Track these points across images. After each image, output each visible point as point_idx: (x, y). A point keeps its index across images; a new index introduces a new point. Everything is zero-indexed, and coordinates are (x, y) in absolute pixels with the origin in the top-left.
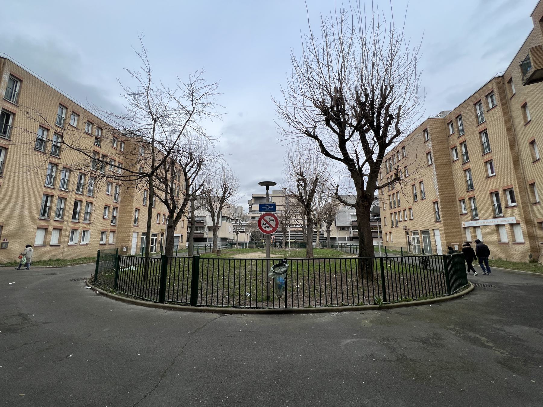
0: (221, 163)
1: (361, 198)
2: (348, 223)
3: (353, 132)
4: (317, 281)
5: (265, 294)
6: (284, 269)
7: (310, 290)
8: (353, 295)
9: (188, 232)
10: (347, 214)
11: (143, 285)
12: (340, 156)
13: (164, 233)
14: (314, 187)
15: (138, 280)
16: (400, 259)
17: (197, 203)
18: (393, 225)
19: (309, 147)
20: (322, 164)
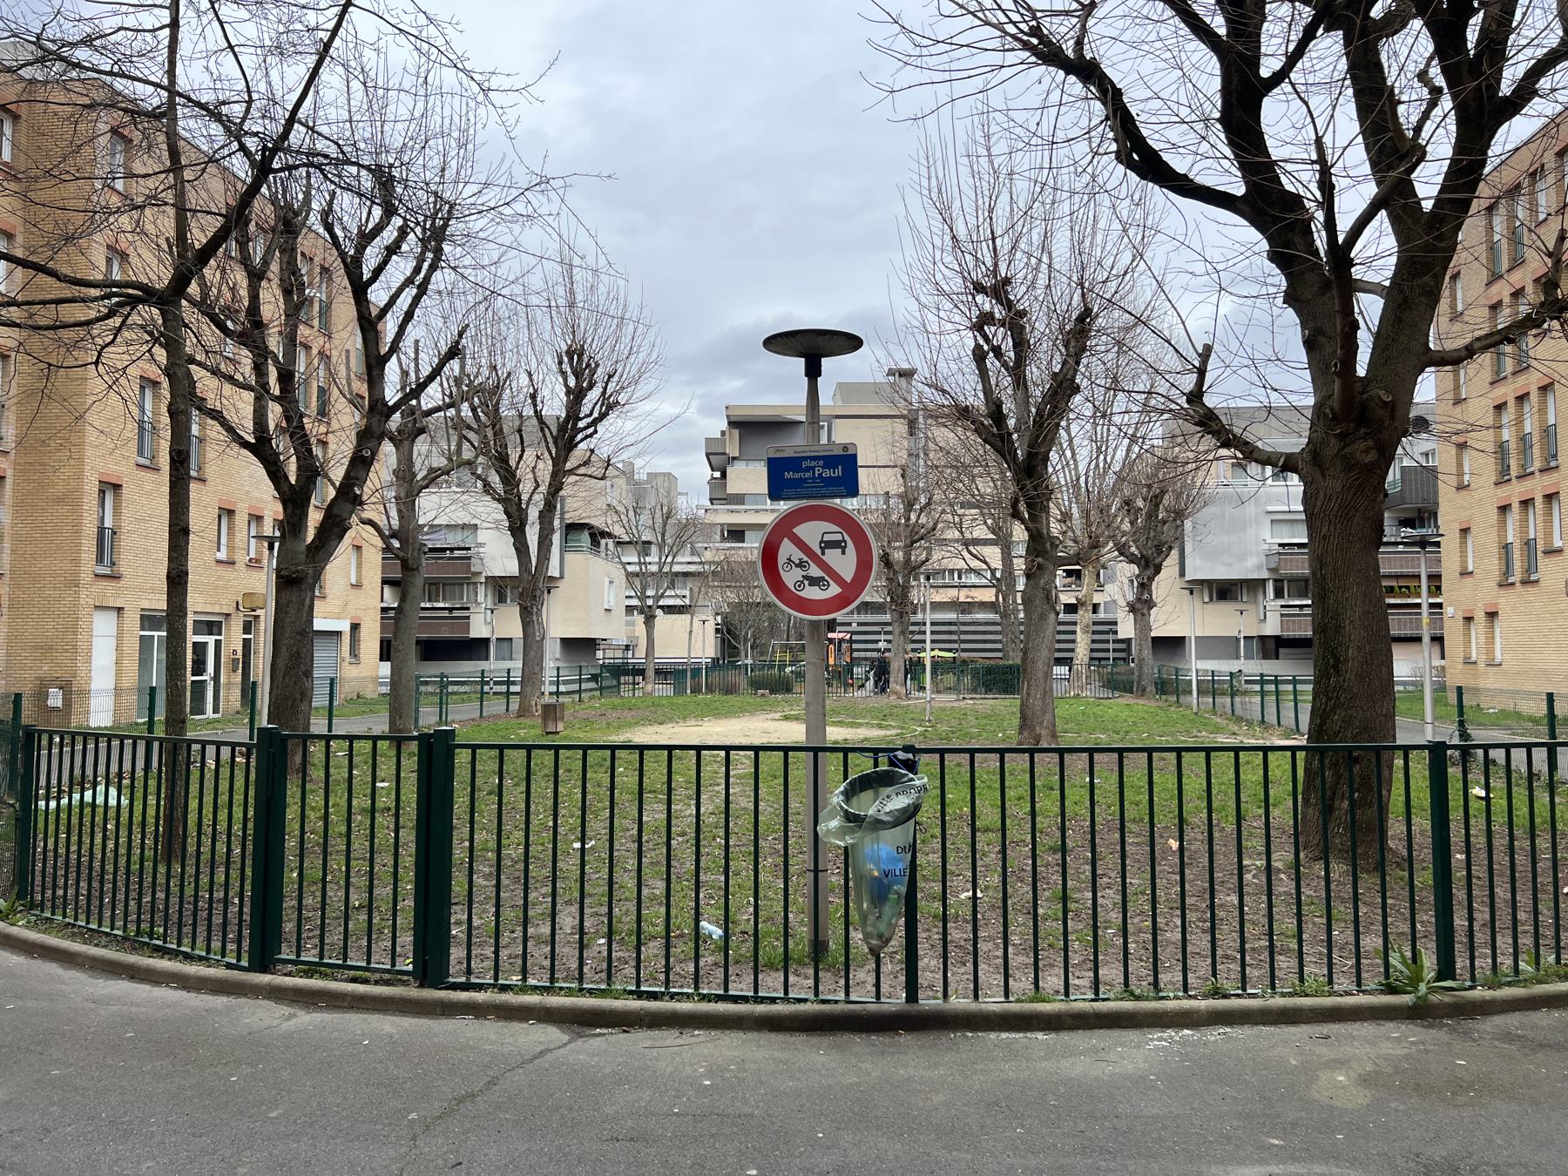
0: (555, 225)
1: (1335, 418)
2: (1252, 562)
3: (1309, 34)
4: (1080, 869)
5: (802, 929)
6: (900, 802)
7: (1040, 911)
8: (1271, 941)
9: (384, 610)
10: (1250, 509)
11: (161, 879)
12: (1226, 179)
13: (258, 612)
14: (1071, 361)
15: (135, 858)
16: (1540, 755)
17: (427, 454)
18: (1507, 570)
19: (1045, 130)
20: (1117, 226)
